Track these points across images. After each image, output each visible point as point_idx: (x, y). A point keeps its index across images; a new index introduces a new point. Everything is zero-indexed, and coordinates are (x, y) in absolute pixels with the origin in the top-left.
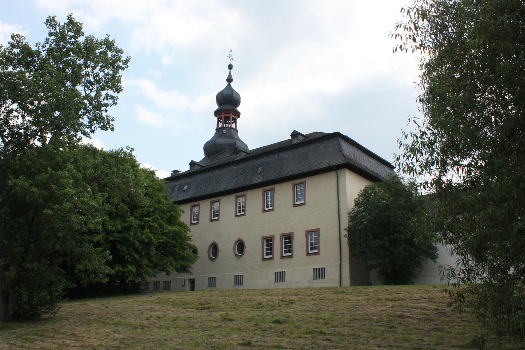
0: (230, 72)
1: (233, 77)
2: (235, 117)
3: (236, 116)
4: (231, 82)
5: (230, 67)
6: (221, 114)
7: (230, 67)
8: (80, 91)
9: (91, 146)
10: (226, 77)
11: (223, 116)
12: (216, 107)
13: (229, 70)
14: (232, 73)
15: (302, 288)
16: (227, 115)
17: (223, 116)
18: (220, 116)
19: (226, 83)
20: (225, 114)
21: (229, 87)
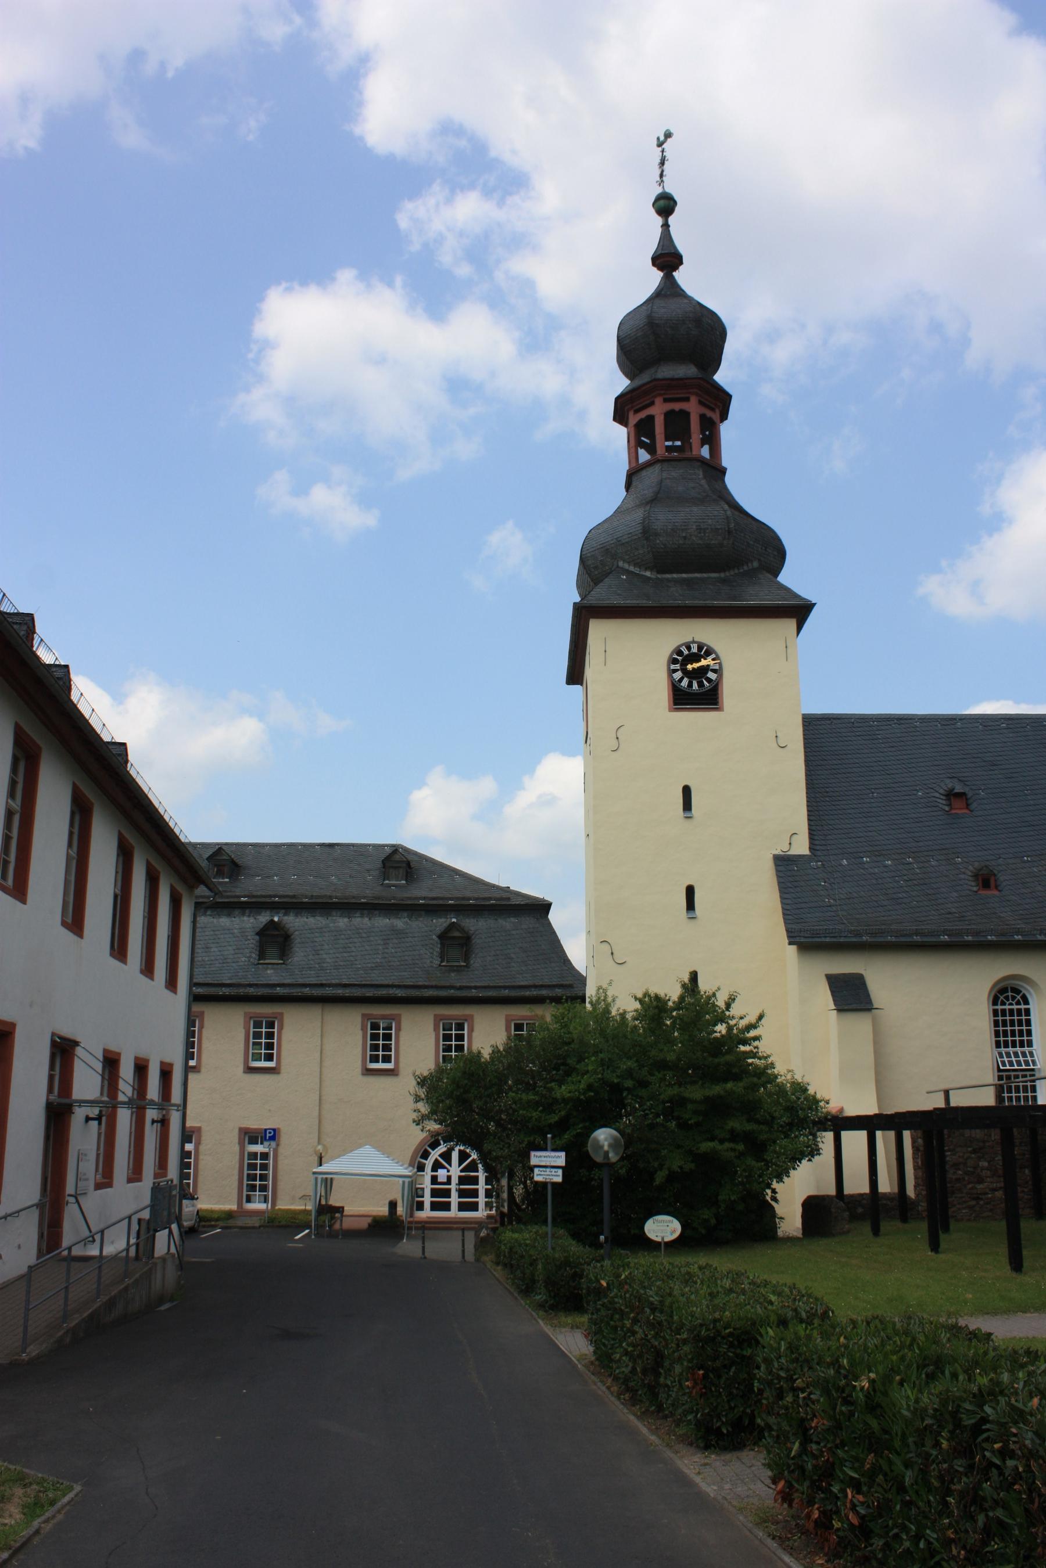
0: (666, 226)
1: (681, 244)
2: (709, 414)
3: (713, 410)
4: (675, 267)
5: (665, 206)
6: (652, 403)
7: (665, 206)
8: (697, 1482)
9: (800, 1088)
10: (652, 245)
11: (658, 410)
12: (811, 1091)
13: (659, 220)
14: (673, 231)
15: (794, 1558)
16: (677, 406)
17: (658, 410)
18: (642, 415)
19: (656, 277)
20: (666, 400)
21: (669, 290)
